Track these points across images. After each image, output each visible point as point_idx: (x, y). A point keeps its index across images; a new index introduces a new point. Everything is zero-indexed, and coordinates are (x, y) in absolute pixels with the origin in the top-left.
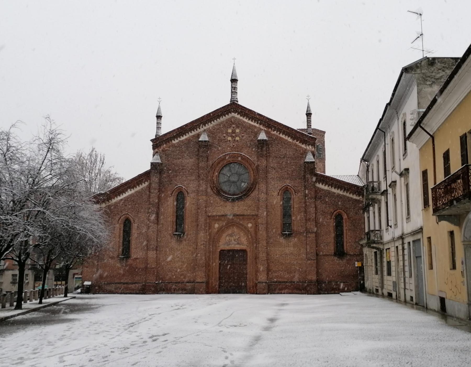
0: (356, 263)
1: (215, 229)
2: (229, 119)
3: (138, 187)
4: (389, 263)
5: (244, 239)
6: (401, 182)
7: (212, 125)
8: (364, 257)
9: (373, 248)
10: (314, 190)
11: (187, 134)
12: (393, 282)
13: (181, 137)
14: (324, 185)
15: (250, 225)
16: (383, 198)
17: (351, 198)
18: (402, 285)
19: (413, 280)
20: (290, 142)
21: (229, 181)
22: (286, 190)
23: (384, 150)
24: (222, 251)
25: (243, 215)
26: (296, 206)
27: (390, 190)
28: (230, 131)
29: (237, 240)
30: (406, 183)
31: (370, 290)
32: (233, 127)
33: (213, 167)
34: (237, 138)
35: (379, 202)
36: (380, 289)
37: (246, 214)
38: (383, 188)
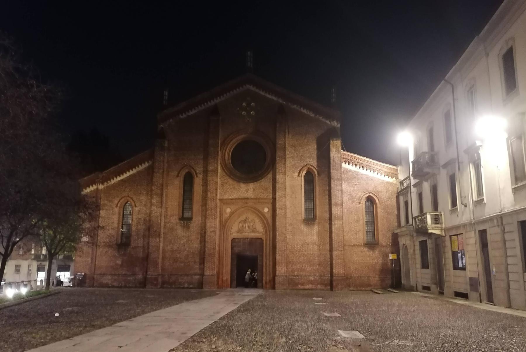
3: (140, 166)
15: (266, 210)
25: (259, 199)
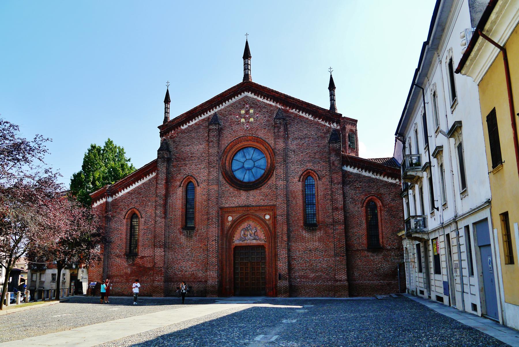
1: (228, 222)
2: (242, 98)
4: (437, 258)
5: (262, 235)
6: (449, 146)
7: (223, 107)
8: (405, 252)
9: (416, 239)
10: (340, 174)
11: (196, 118)
12: (444, 283)
13: (190, 121)
14: (353, 167)
15: (267, 217)
16: (425, 175)
17: (386, 182)
18: (458, 287)
19: (475, 280)
22: (307, 175)
23: (423, 112)
24: (237, 248)
25: (259, 206)
26: (321, 193)
27: (434, 161)
28: (243, 112)
29: (253, 235)
30: (457, 144)
31: (413, 291)
33: (225, 152)
34: (252, 120)
35: (419, 179)
36: (425, 291)
37: (262, 203)
38: (424, 160)
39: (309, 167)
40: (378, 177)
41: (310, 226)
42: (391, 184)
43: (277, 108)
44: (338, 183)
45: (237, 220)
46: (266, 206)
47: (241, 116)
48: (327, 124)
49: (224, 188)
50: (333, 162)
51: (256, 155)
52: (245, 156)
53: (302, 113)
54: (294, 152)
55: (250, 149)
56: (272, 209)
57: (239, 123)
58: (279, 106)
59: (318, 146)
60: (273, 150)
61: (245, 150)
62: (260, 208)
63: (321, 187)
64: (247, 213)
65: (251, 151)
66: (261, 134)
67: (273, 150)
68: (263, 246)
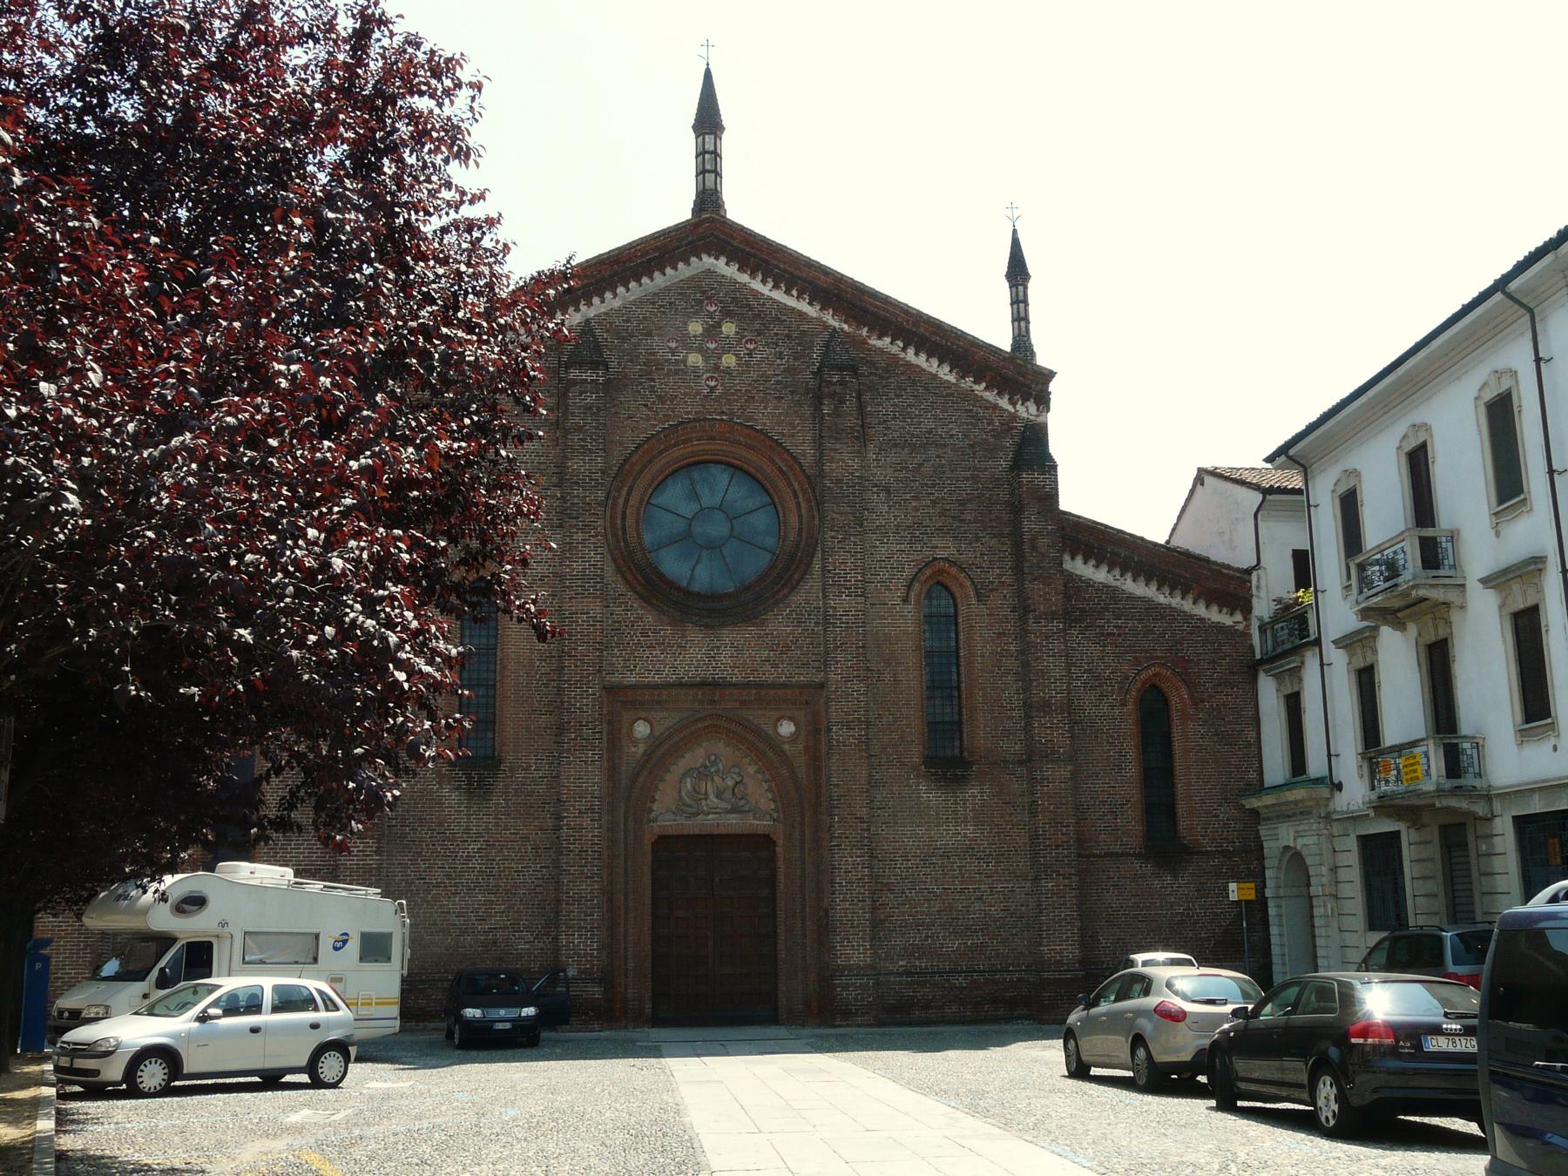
0: (1233, 886)
1: (635, 742)
2: (692, 278)
5: (760, 795)
7: (617, 303)
14: (1092, 562)
15: (787, 728)
17: (1202, 620)
20: (948, 384)
21: (687, 536)
24: (665, 843)
25: (759, 686)
28: (696, 328)
29: (728, 795)
32: (711, 315)
37: (770, 676)
39: (941, 554)
40: (1176, 601)
41: (948, 761)
42: (1220, 628)
43: (826, 327)
44: (1052, 616)
45: (670, 736)
46: (784, 686)
47: (687, 343)
48: (1004, 403)
49: (619, 610)
50: (1034, 539)
51: (739, 494)
52: (694, 496)
53: (916, 354)
54: (888, 492)
55: (714, 469)
56: (808, 699)
57: (680, 369)
58: (830, 319)
59: (974, 479)
60: (808, 477)
61: (695, 474)
62: (759, 692)
63: (983, 630)
64: (718, 708)
65: (722, 478)
66: (765, 416)
67: (808, 477)
68: (766, 837)
